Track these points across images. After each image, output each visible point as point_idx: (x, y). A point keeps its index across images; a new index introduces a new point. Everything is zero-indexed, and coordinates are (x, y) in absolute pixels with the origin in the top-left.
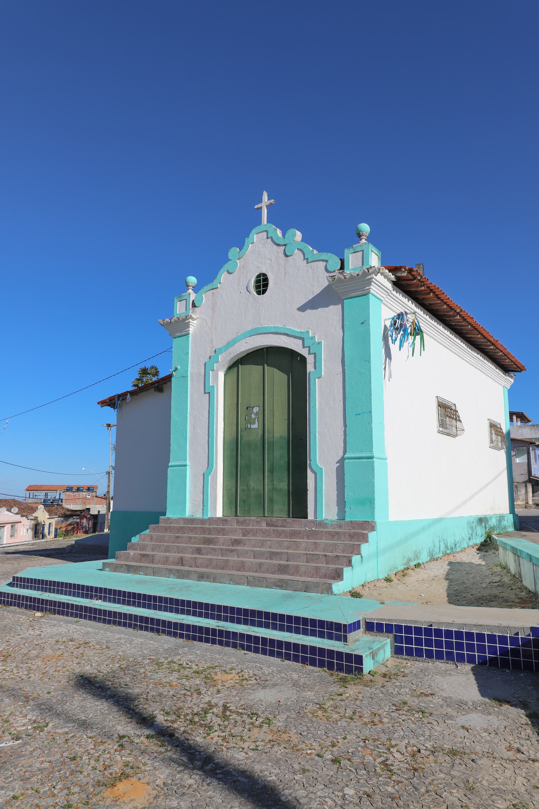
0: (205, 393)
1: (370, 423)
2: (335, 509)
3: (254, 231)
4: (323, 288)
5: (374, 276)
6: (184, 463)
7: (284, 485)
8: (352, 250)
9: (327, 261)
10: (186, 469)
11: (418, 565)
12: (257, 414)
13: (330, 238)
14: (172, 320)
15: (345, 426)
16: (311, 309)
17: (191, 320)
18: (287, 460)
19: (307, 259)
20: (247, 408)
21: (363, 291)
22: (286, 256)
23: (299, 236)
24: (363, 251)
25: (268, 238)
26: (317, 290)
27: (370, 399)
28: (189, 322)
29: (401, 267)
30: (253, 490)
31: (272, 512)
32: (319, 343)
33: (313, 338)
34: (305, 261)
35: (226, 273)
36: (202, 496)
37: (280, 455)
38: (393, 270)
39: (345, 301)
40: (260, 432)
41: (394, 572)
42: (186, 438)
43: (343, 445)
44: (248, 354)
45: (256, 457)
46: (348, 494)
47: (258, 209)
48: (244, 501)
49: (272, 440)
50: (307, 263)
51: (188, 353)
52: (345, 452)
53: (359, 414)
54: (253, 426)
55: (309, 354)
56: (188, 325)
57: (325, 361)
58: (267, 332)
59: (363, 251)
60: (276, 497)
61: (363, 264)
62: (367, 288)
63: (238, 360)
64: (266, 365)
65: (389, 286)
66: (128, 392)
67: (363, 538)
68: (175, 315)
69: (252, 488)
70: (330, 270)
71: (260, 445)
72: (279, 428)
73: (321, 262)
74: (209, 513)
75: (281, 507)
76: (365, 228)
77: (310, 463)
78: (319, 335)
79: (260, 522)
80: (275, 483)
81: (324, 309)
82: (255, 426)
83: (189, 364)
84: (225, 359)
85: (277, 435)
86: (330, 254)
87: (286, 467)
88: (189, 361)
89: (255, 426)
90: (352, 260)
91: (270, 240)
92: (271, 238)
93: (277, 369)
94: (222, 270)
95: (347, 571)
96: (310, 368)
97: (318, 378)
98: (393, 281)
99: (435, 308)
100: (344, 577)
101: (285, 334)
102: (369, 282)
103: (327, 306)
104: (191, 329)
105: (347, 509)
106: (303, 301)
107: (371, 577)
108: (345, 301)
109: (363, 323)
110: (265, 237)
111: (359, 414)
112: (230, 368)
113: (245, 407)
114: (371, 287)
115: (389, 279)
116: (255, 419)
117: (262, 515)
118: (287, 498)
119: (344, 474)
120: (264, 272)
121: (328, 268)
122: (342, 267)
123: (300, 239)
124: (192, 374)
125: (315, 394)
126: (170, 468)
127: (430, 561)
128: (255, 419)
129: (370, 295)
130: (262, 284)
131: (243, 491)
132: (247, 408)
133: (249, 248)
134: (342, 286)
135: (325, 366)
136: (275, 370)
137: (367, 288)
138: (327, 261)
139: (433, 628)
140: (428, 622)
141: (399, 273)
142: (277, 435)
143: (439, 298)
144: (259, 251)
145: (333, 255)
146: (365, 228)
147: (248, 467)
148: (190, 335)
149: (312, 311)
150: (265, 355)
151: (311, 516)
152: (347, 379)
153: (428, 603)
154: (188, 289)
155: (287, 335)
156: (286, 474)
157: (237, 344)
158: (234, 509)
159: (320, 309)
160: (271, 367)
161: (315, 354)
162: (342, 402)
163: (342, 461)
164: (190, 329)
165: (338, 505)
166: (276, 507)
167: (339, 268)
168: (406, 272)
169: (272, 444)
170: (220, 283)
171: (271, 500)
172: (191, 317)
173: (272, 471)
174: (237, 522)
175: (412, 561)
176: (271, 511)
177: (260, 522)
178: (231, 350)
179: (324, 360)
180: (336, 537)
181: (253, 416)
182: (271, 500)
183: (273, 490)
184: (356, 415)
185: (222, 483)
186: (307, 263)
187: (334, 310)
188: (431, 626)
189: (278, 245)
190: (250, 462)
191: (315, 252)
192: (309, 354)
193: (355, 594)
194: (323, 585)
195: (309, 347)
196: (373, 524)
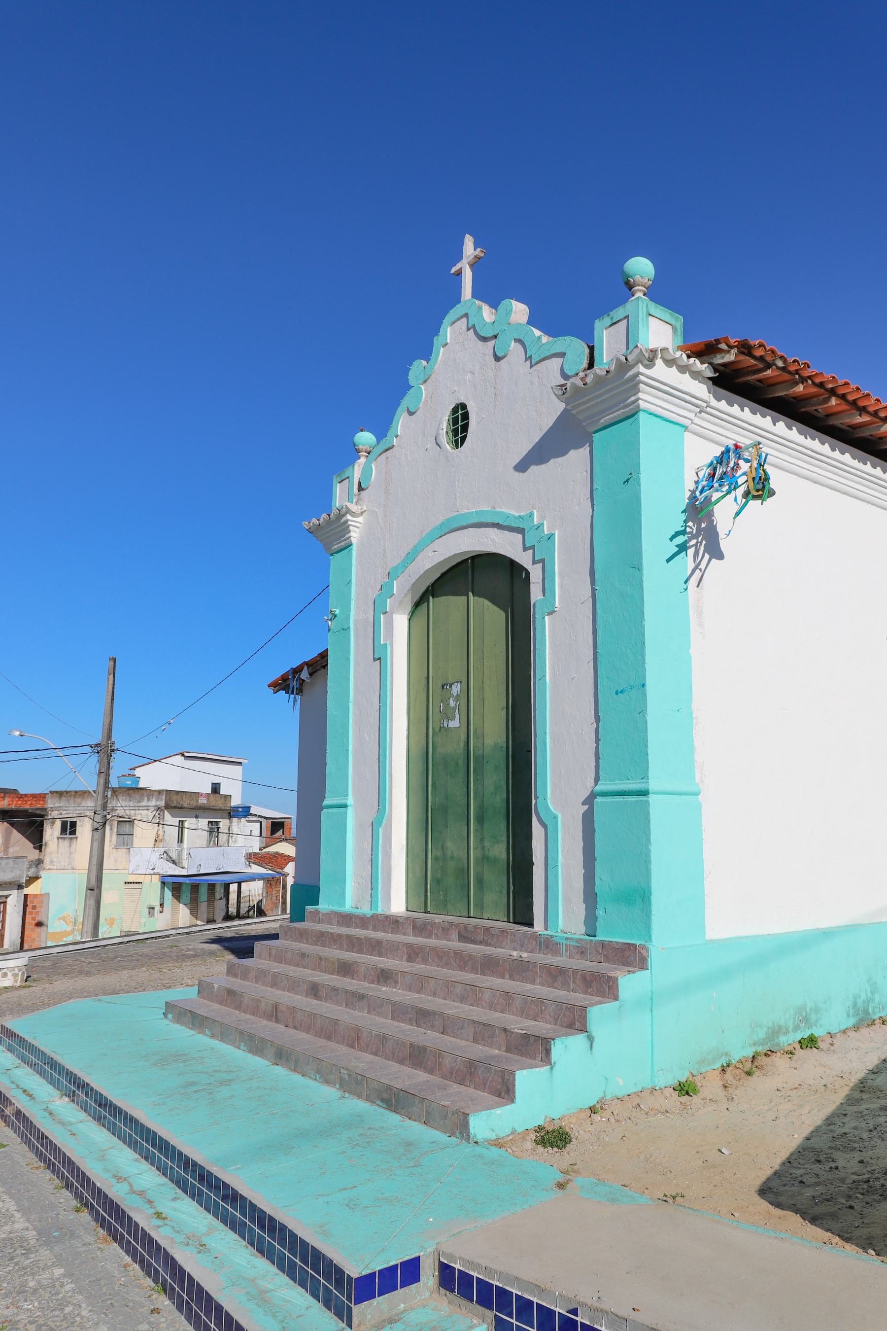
0: (375, 660)
1: (643, 712)
2: (580, 910)
3: (447, 320)
4: (559, 414)
5: (642, 369)
6: (343, 802)
8: (607, 321)
9: (562, 355)
10: (346, 813)
11: (810, 1042)
13: (571, 304)
14: (322, 520)
15: (597, 719)
16: (537, 464)
17: (349, 517)
18: (505, 795)
19: (531, 357)
20: (443, 686)
21: (626, 406)
22: (498, 359)
23: (519, 311)
24: (627, 317)
25: (468, 329)
26: (548, 422)
27: (643, 656)
28: (347, 521)
29: (718, 341)
30: (452, 858)
31: (482, 908)
32: (551, 537)
33: (539, 527)
34: (528, 362)
35: (406, 414)
36: (369, 867)
37: (494, 784)
38: (704, 351)
39: (596, 436)
40: (463, 737)
41: (718, 1065)
43: (594, 764)
49: (481, 752)
51: (350, 582)
53: (622, 692)
55: (535, 562)
57: (561, 577)
59: (627, 317)
62: (633, 398)
63: (428, 588)
64: (470, 594)
65: (701, 390)
67: (610, 988)
68: (334, 508)
69: (449, 853)
71: (462, 763)
73: (554, 359)
74: (379, 904)
75: (496, 896)
76: (641, 267)
77: (536, 803)
78: (545, 515)
80: (487, 844)
83: (353, 603)
84: (403, 588)
85: (489, 742)
86: (568, 339)
87: (504, 811)
88: (353, 597)
89: (454, 724)
90: (608, 342)
92: (474, 326)
93: (490, 600)
94: (399, 409)
95: (526, 1080)
96: (535, 594)
97: (550, 613)
98: (709, 378)
99: (865, 433)
100: (517, 1095)
102: (633, 385)
103: (563, 453)
104: (355, 535)
107: (623, 1084)
109: (627, 481)
110: (464, 328)
111: (622, 692)
112: (417, 605)
113: (440, 685)
114: (641, 395)
115: (695, 375)
117: (465, 914)
119: (594, 831)
122: (591, 365)
123: (524, 319)
124: (356, 621)
125: (545, 651)
126: (325, 810)
127: (856, 1028)
129: (641, 414)
131: (436, 859)
132: (443, 686)
133: (440, 354)
134: (584, 403)
135: (561, 586)
136: (486, 602)
137: (633, 398)
138: (562, 355)
139: (579, 1319)
140: (570, 1300)
141: (719, 356)
142: (489, 742)
143: (863, 410)
145: (575, 339)
146: (641, 267)
148: (354, 547)
149: (539, 466)
150: (470, 573)
151: (538, 926)
152: (599, 611)
153: (679, 1199)
154: (359, 458)
157: (420, 557)
158: (423, 897)
159: (552, 461)
160: (480, 597)
161: (542, 561)
163: (590, 800)
164: (352, 534)
168: (734, 351)
169: (480, 759)
170: (397, 436)
171: (480, 882)
172: (348, 511)
173: (480, 820)
174: (414, 927)
175: (787, 1033)
176: (480, 905)
179: (560, 573)
180: (560, 979)
181: (452, 703)
183: (484, 859)
184: (617, 693)
185: (404, 843)
186: (531, 366)
187: (578, 457)
188: (575, 1312)
189: (484, 339)
190: (447, 799)
191: (545, 339)
192: (535, 562)
193: (553, 1138)
194: (453, 1114)
195: (533, 547)
196: (643, 952)
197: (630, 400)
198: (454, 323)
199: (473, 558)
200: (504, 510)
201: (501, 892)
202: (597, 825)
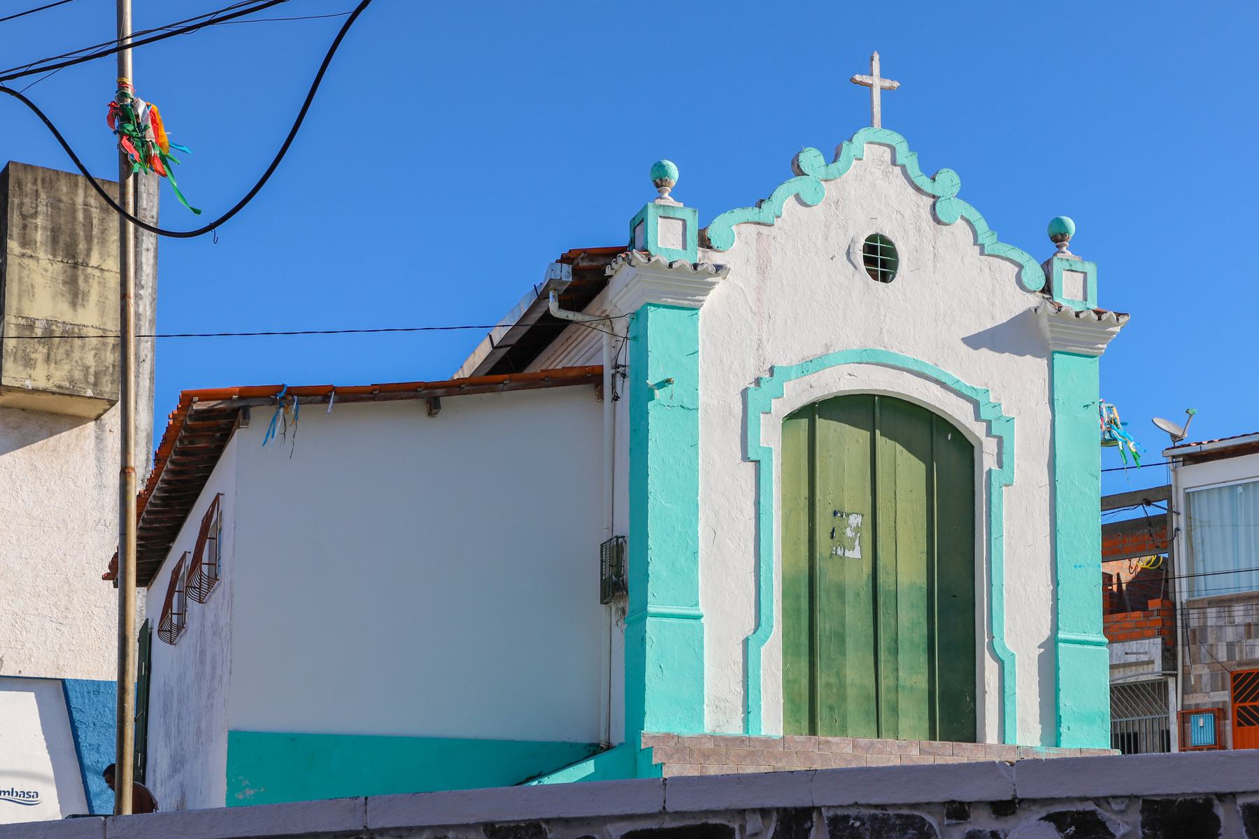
7: (922, 681)
9: (1021, 267)
12: (857, 529)
15: (1055, 582)
20: (835, 513)
26: (1002, 318)
34: (977, 248)
36: (740, 689)
37: (910, 619)
39: (1057, 356)
40: (867, 569)
42: (696, 553)
45: (856, 617)
46: (1066, 702)
47: (861, 83)
48: (831, 708)
49: (893, 588)
50: (982, 253)
52: (1055, 628)
54: (848, 554)
56: (707, 288)
60: (902, 705)
61: (1085, 299)
63: (813, 404)
66: (333, 388)
69: (849, 680)
72: (909, 568)
79: (906, 747)
82: (855, 554)
89: (855, 554)
91: (897, 170)
96: (987, 461)
97: (1007, 485)
101: (937, 382)
103: (1022, 354)
105: (1063, 730)
106: (974, 330)
108: (1057, 356)
112: (793, 416)
113: (830, 510)
116: (853, 540)
118: (925, 707)
120: (887, 233)
121: (1025, 279)
128: (853, 540)
130: (880, 259)
136: (899, 447)
142: (904, 580)
144: (871, 182)
147: (840, 638)
148: (700, 312)
149: (992, 353)
152: (1059, 499)
155: (943, 385)
156: (924, 659)
157: (827, 370)
162: (1048, 539)
165: (1042, 720)
166: (904, 723)
177: (906, 747)
178: (812, 379)
181: (849, 533)
182: (895, 710)
190: (843, 626)
192: (989, 433)
199: (880, 396)
201: (920, 718)
202: (1061, 664)
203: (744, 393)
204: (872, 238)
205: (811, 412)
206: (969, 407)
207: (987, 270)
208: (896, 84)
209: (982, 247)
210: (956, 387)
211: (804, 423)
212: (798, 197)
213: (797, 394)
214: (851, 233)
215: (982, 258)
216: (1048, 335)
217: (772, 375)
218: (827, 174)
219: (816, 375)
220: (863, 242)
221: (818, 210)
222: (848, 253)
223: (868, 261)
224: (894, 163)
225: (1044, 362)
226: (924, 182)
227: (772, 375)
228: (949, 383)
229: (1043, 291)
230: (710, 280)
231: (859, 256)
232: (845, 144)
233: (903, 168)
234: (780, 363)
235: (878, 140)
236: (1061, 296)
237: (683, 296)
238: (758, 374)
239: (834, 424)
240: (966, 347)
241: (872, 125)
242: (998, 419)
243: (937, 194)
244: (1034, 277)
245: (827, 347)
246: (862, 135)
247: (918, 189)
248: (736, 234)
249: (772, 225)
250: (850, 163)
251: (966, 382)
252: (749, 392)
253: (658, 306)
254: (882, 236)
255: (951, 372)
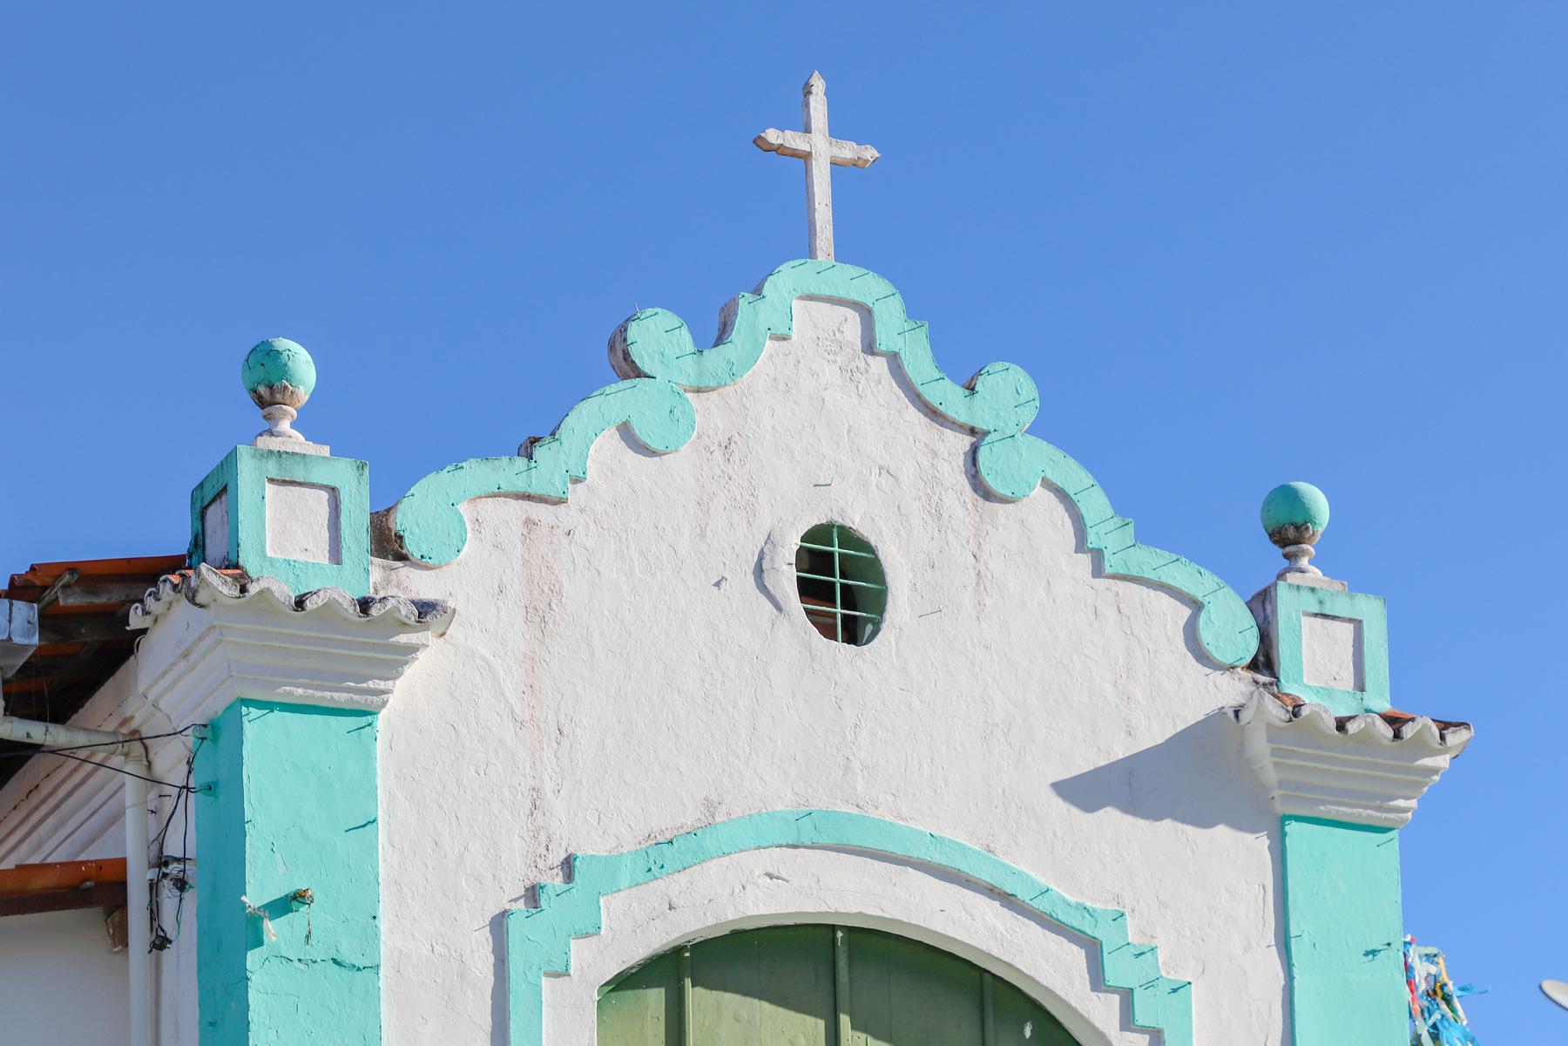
9: (1196, 606)
21: (1379, 809)
26: (1153, 733)
34: (1085, 560)
39: (1293, 828)
44: (736, 934)
47: (780, 150)
50: (1098, 571)
58: (899, 851)
62: (382, 685)
63: (678, 951)
64: (688, 982)
70: (1218, 656)
81: (1190, 829)
91: (879, 365)
101: (992, 892)
103: (1204, 820)
108: (1293, 828)
109: (1373, 952)
121: (1206, 636)
130: (839, 585)
137: (382, 685)
144: (809, 395)
148: (381, 721)
149: (1129, 819)
155: (1008, 900)
157: (713, 866)
159: (1167, 823)
167: (1249, 659)
178: (673, 886)
197: (371, 684)
198: (810, 298)
199: (850, 930)
200: (1027, 871)
203: (499, 925)
204: (819, 533)
205: (671, 970)
206: (1076, 956)
207: (1112, 613)
208: (870, 153)
209: (1098, 556)
210: (1041, 905)
211: (655, 998)
212: (626, 432)
213: (636, 927)
214: (765, 522)
215: (1100, 583)
216: (1271, 776)
217: (569, 877)
218: (700, 375)
219: (683, 878)
220: (794, 542)
221: (681, 462)
222: (759, 571)
223: (807, 590)
224: (870, 348)
225: (1261, 843)
226: (947, 396)
227: (569, 877)
228: (1023, 895)
229: (1253, 666)
230: (403, 639)
231: (786, 579)
232: (745, 302)
233: (894, 360)
234: (590, 846)
235: (828, 292)
236: (1298, 680)
237: (335, 680)
238: (534, 877)
239: (730, 999)
240: (1061, 806)
241: (811, 253)
242: (1150, 985)
243: (980, 425)
244: (1232, 632)
245: (710, 806)
246: (786, 280)
247: (934, 414)
248: (464, 520)
249: (561, 501)
250: (759, 347)
251: (1066, 892)
252: (513, 924)
253: (269, 706)
254: (842, 528)
255: (1027, 869)
